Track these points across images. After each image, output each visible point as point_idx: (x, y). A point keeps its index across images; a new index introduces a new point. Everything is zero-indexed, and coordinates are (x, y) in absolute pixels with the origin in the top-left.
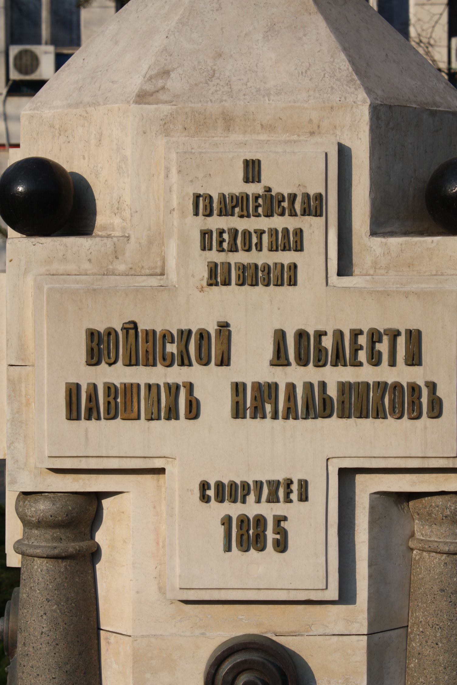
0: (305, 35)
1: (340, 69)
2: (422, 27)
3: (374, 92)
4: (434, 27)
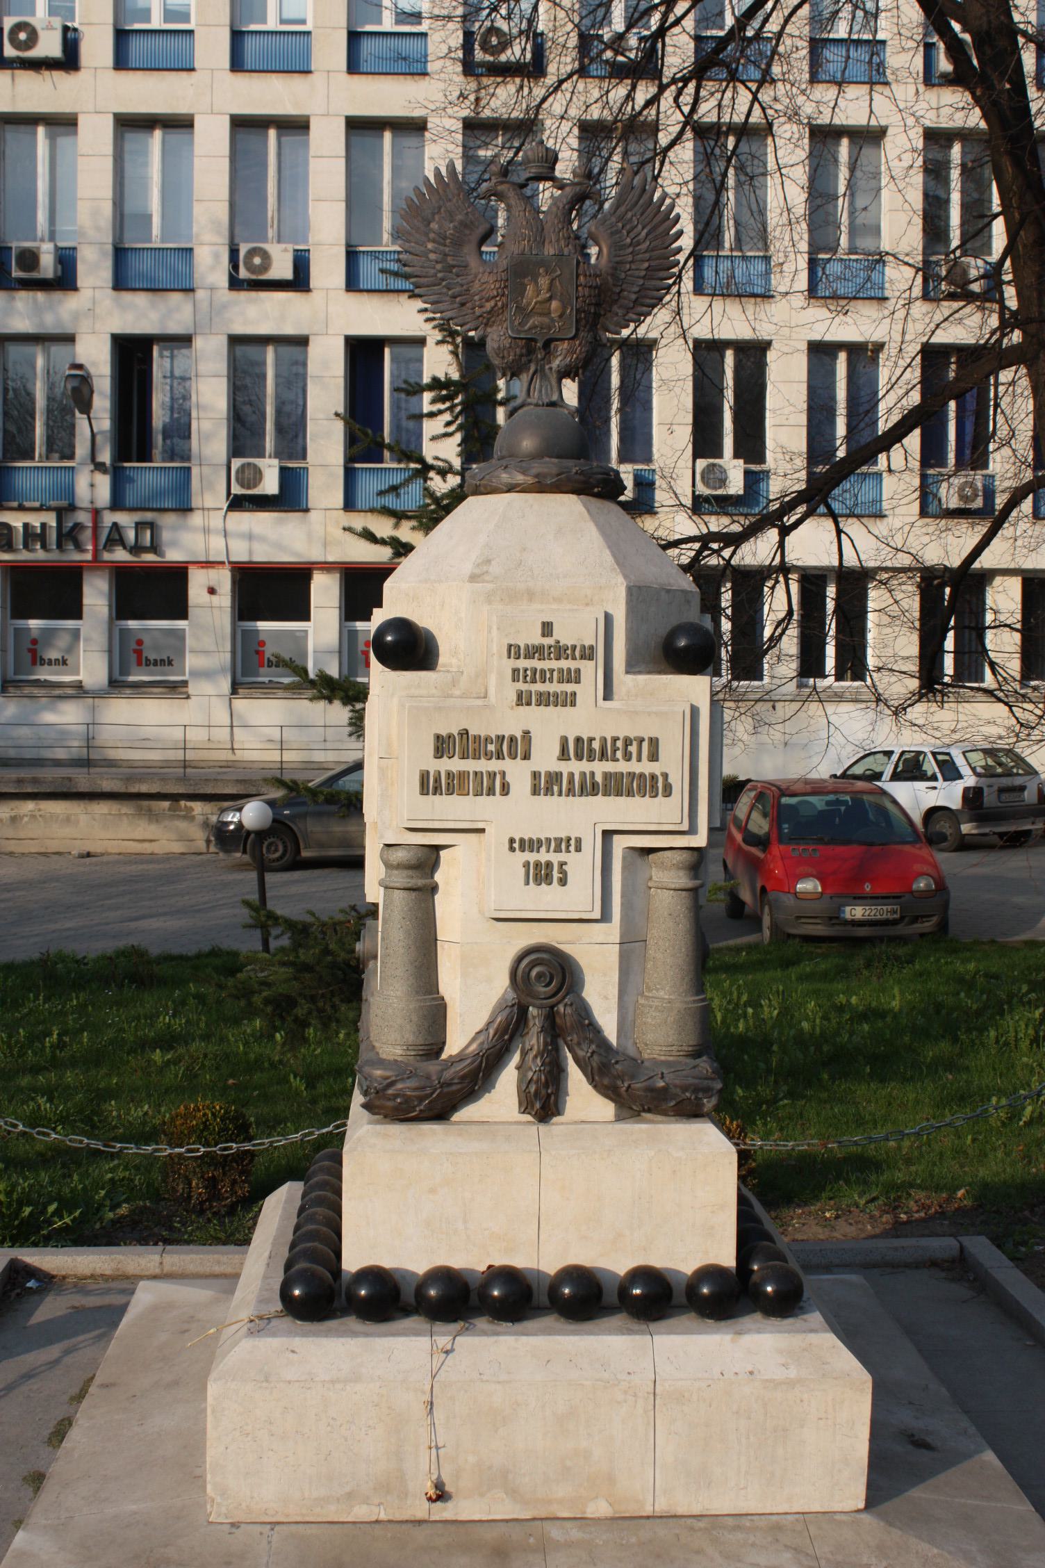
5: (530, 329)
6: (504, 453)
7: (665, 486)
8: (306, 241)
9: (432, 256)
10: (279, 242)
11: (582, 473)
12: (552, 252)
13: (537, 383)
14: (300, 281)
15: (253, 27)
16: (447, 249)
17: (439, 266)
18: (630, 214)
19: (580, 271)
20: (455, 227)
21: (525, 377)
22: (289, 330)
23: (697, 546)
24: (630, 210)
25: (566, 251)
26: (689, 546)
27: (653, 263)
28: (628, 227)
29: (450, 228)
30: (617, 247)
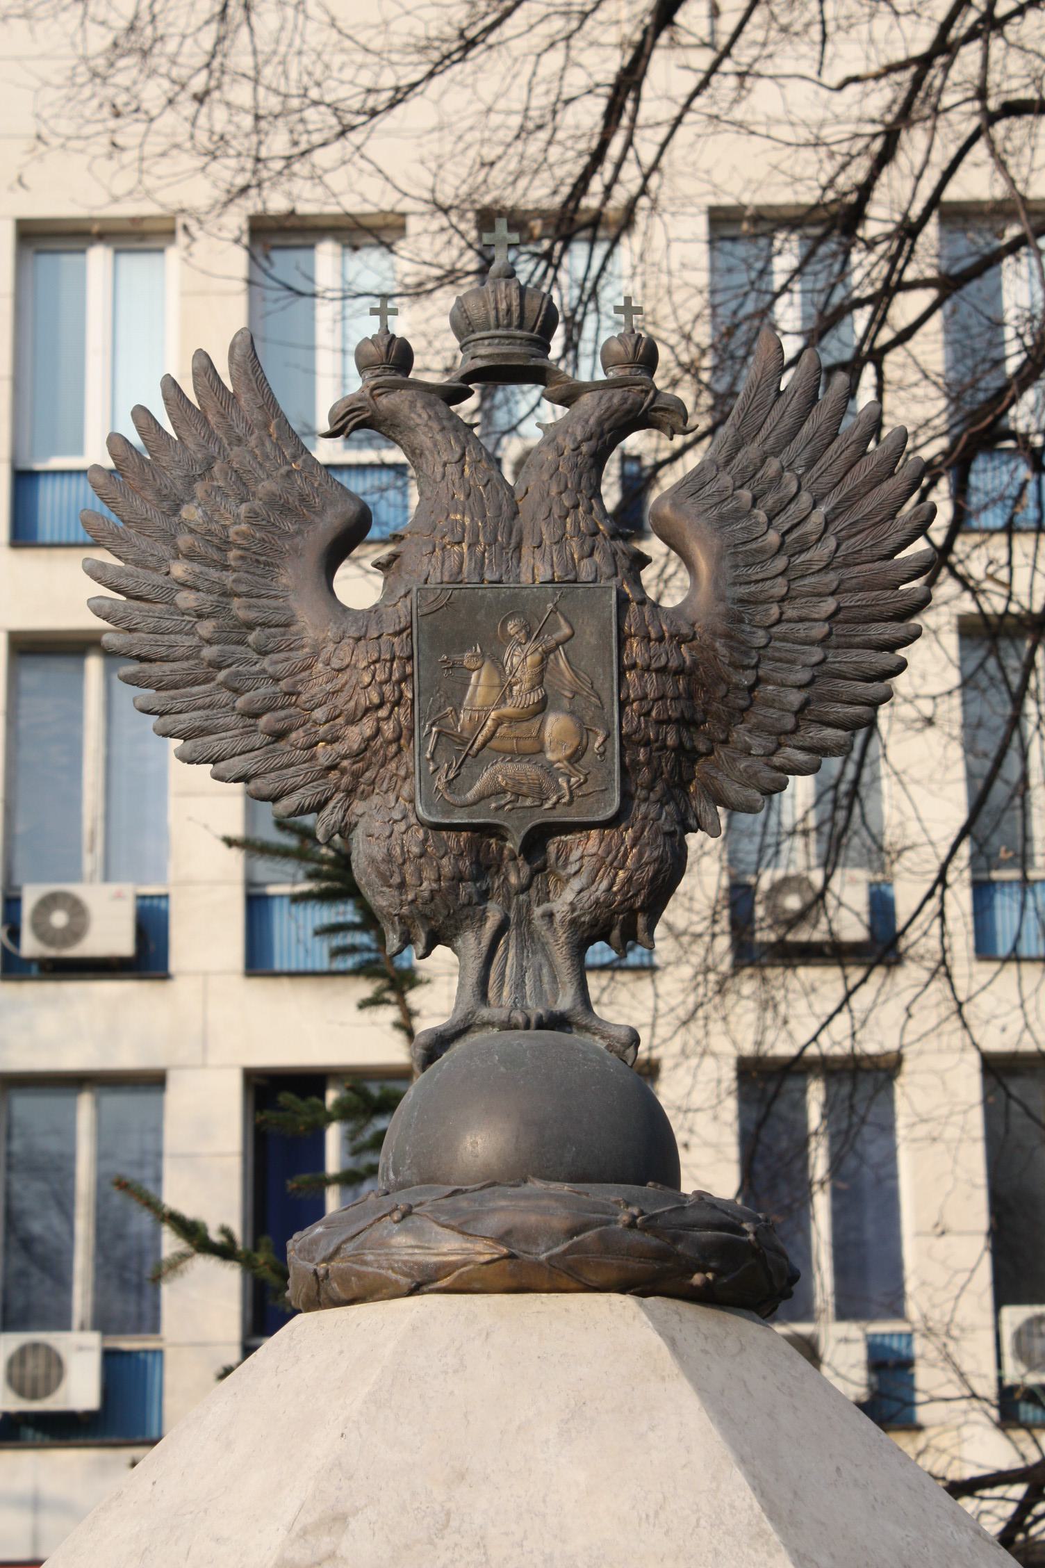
0: (652, 1428)
1: (732, 1506)
2: (930, 1299)
3: (812, 1561)
4: (958, 1297)
5: (482, 798)
6: (407, 1174)
7: (933, 1354)
8: (160, 873)
9: (186, 599)
10: (107, 878)
11: (650, 1224)
12: (543, 573)
13: (509, 956)
14: (148, 958)
15: (57, 463)
16: (229, 578)
17: (206, 628)
18: (773, 465)
19: (631, 625)
20: (253, 517)
21: (473, 942)
22: (126, 1059)
23: (1018, 1491)
24: (776, 453)
25: (585, 570)
26: (998, 1491)
27: (848, 600)
28: (770, 500)
29: (236, 520)
30: (739, 556)
